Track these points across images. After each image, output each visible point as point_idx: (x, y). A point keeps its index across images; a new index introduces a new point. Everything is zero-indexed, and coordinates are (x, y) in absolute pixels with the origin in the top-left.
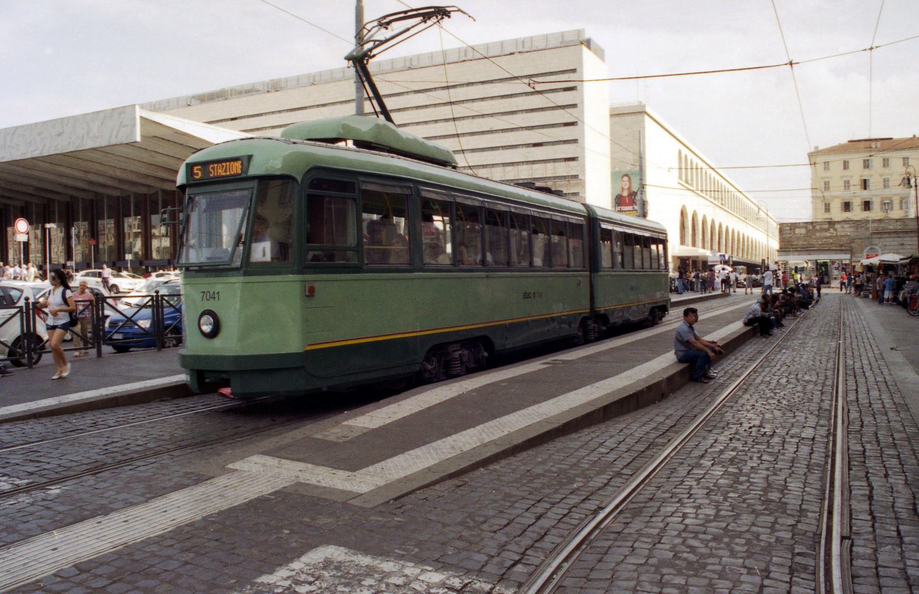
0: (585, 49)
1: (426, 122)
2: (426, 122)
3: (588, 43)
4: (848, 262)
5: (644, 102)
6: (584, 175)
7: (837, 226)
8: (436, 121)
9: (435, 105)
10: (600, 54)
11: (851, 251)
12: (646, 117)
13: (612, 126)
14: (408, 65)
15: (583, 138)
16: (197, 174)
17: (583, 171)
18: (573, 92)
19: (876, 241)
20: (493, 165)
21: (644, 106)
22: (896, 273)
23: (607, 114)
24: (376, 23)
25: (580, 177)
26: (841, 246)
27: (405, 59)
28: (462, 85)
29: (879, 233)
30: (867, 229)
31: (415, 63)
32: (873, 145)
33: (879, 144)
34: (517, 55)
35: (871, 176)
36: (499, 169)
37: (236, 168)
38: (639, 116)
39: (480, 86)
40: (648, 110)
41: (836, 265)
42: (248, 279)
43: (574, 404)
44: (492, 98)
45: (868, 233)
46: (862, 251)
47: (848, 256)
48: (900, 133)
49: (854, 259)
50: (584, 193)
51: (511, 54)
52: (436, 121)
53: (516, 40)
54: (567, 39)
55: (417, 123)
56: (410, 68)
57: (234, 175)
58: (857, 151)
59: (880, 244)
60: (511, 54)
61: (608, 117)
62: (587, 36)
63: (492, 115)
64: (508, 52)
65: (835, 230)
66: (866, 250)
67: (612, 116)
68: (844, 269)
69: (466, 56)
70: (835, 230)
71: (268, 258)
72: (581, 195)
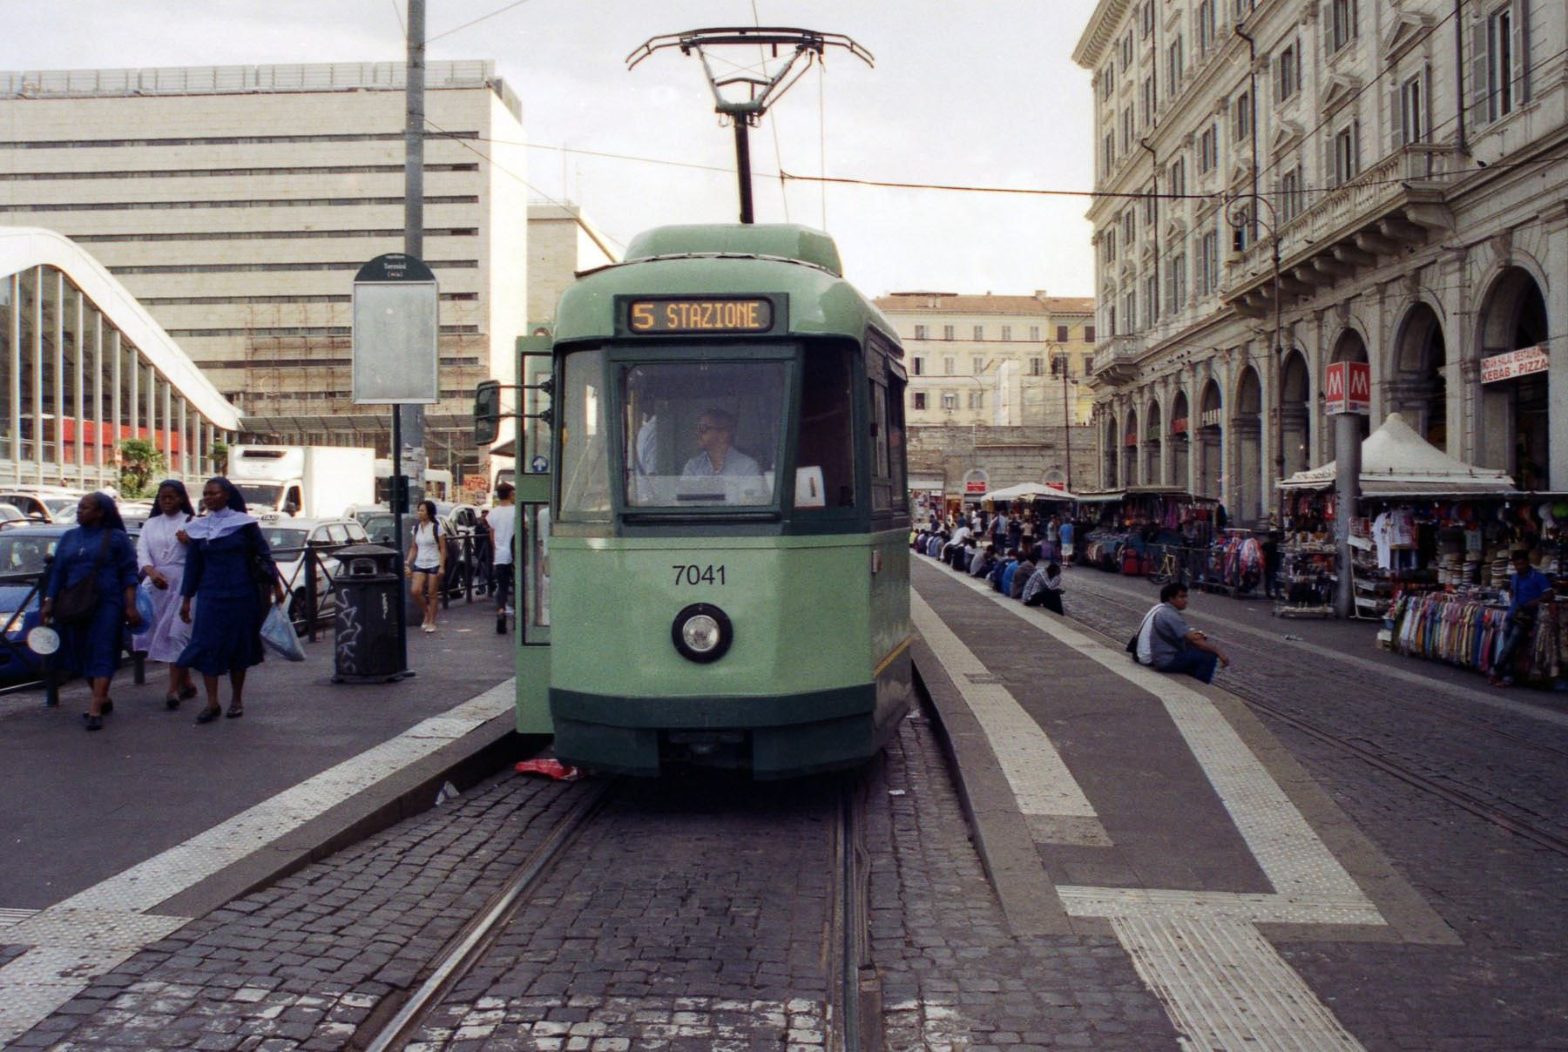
0: (494, 96)
1: (172, 205)
2: (172, 205)
3: (497, 86)
4: (939, 494)
5: (575, 203)
6: (488, 327)
7: (922, 434)
8: (193, 204)
9: (192, 172)
10: (514, 106)
11: (944, 476)
12: (580, 230)
13: (532, 239)
14: (133, 86)
15: (488, 260)
16: (645, 321)
17: (487, 318)
18: (472, 174)
19: (983, 461)
20: (310, 298)
21: (577, 209)
22: (1074, 515)
23: (523, 218)
24: (677, 40)
25: (481, 330)
26: (929, 466)
27: (127, 74)
28: (250, 139)
29: (987, 449)
30: (968, 440)
31: (148, 85)
32: (931, 302)
33: (939, 301)
34: (362, 93)
35: (927, 353)
36: (321, 307)
37: (746, 317)
38: (568, 227)
39: (287, 146)
40: (583, 216)
41: (921, 499)
42: (789, 541)
43: (1243, 755)
44: (311, 170)
45: (970, 447)
46: (960, 478)
47: (940, 485)
48: (970, 286)
49: (949, 489)
50: (487, 359)
51: (351, 90)
52: (193, 204)
53: (362, 66)
54: (459, 75)
55: (152, 205)
56: (137, 94)
57: (735, 330)
58: (906, 311)
59: (989, 466)
60: (351, 90)
61: (525, 222)
62: (498, 73)
63: (310, 202)
64: (345, 87)
65: (920, 440)
66: (966, 475)
67: (531, 221)
68: (933, 506)
69: (257, 83)
70: (920, 440)
71: (820, 500)
72: (481, 362)
